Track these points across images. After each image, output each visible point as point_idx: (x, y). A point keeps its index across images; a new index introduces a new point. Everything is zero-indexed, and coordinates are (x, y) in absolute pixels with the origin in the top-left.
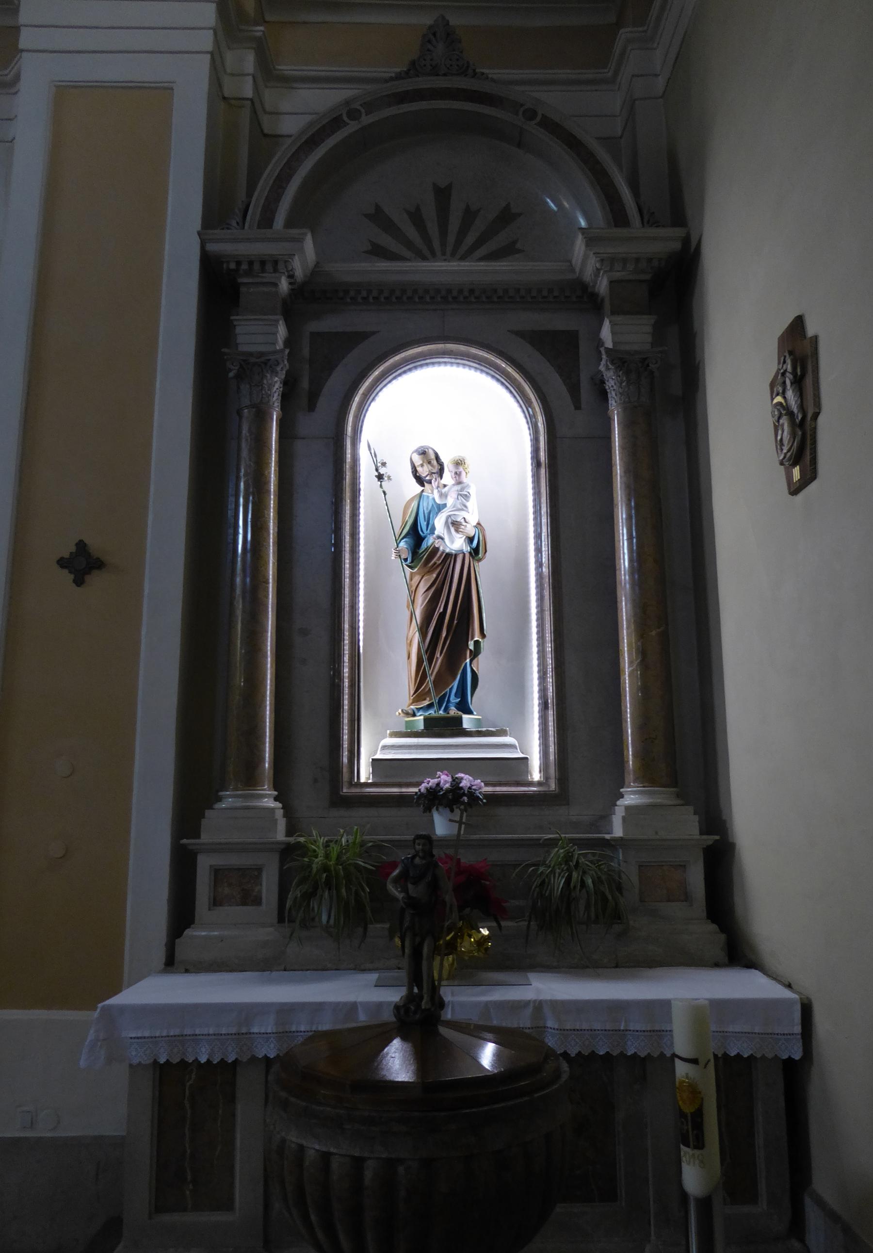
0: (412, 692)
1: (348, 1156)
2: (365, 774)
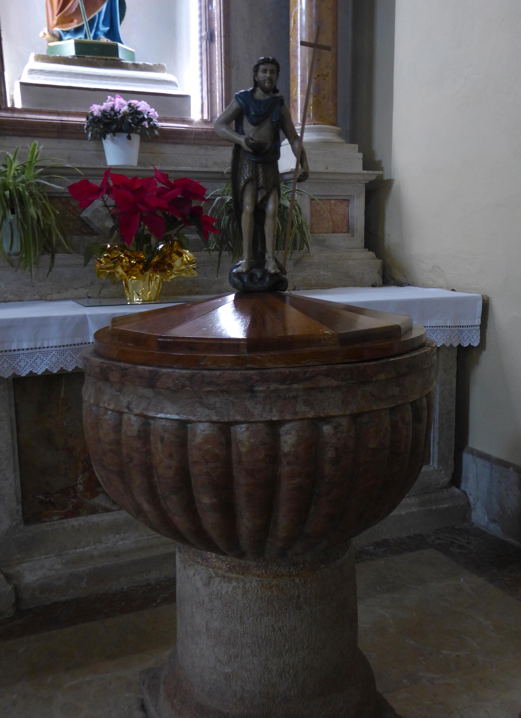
0: (56, 12)
1: (263, 422)
2: (15, 97)
